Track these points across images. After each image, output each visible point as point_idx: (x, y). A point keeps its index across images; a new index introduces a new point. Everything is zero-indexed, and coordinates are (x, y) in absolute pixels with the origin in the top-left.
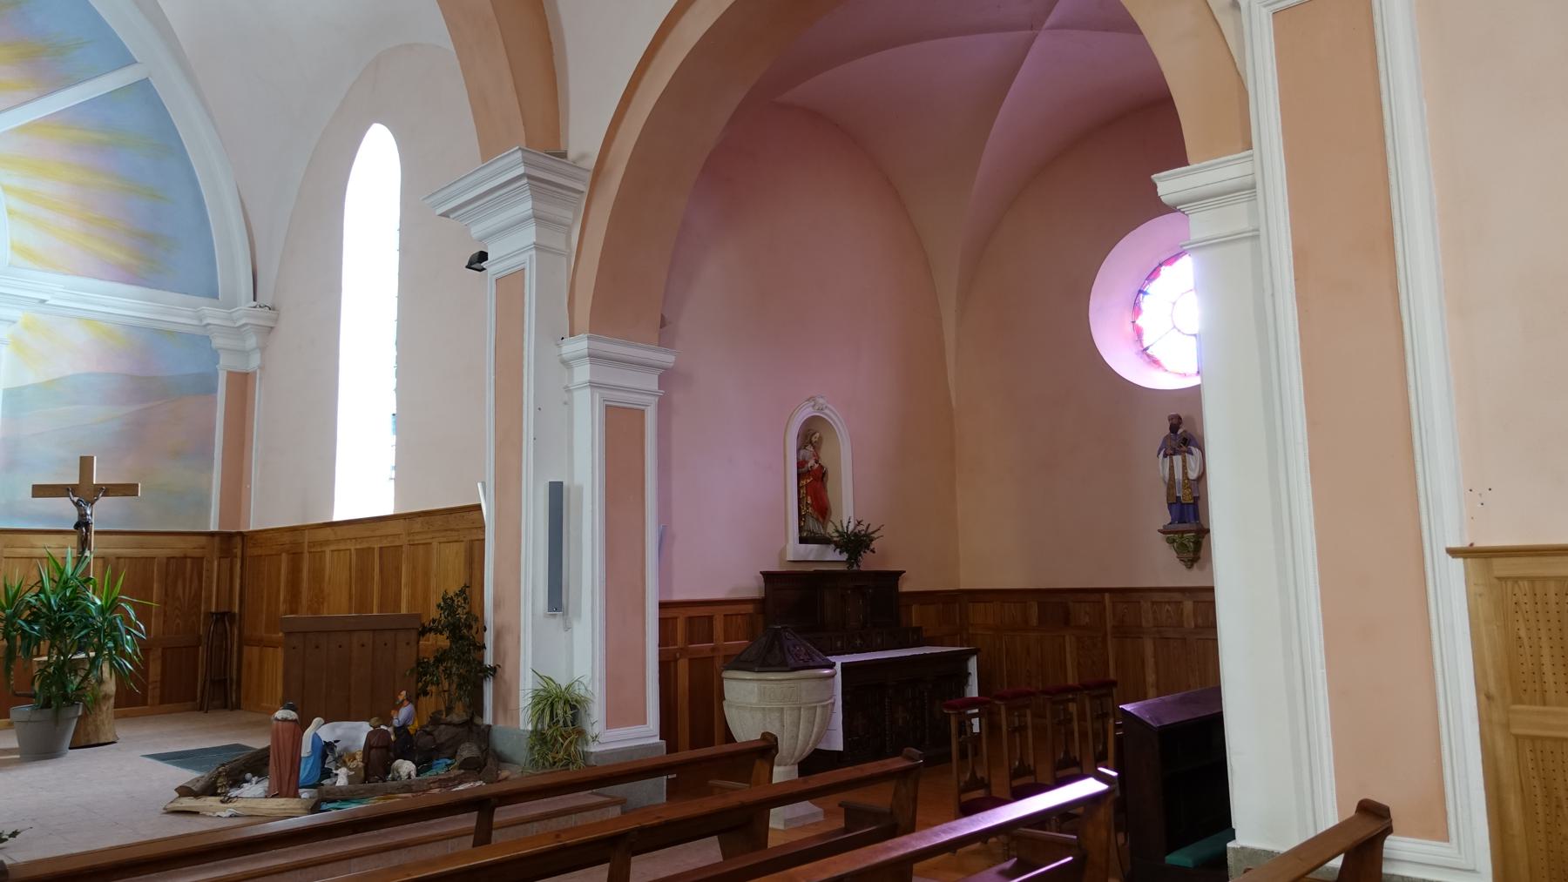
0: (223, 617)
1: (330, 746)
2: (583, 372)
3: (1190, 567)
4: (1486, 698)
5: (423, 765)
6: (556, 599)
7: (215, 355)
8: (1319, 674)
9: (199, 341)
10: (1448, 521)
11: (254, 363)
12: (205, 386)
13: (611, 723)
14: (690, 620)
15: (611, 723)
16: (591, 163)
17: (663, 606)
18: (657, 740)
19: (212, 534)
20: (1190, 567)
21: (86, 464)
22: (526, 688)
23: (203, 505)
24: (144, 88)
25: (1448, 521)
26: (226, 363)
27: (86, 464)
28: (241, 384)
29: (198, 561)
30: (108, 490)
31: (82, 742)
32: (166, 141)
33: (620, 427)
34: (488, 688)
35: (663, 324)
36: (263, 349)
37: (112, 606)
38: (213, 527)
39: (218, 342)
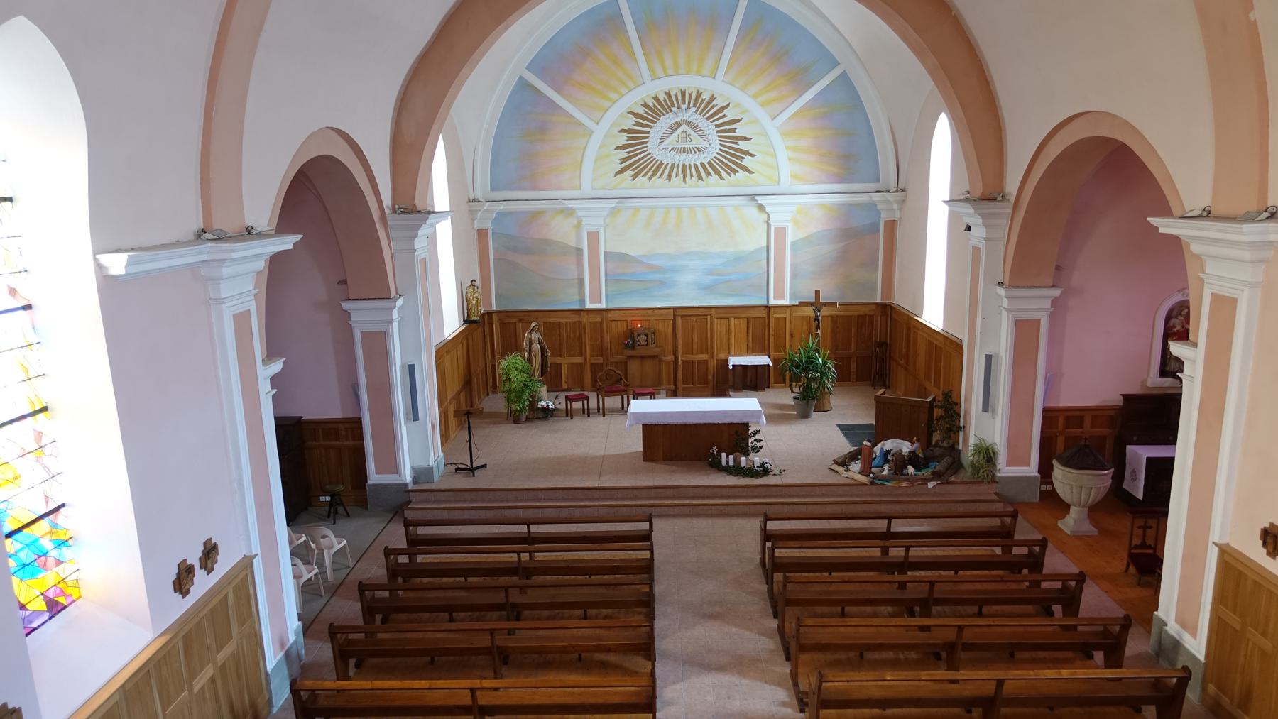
0: (882, 345)
1: (888, 452)
2: (1005, 303)
3: (20, 709)
4: (1214, 599)
5: (917, 468)
6: (986, 407)
7: (878, 213)
8: (1179, 567)
9: (872, 206)
10: (1216, 535)
11: (897, 215)
12: (874, 229)
13: (1010, 463)
14: (1068, 419)
15: (1010, 463)
16: (1013, 199)
17: (1045, 411)
18: (1037, 474)
19: (877, 304)
20: (20, 709)
21: (817, 292)
22: (972, 441)
23: (874, 289)
24: (844, 77)
25: (1216, 535)
26: (884, 216)
27: (817, 292)
28: (891, 226)
29: (871, 316)
30: (826, 304)
31: (819, 409)
32: (855, 103)
33: (1025, 331)
34: (961, 434)
35: (1058, 268)
36: (901, 209)
37: (825, 363)
38: (879, 300)
39: (879, 207)
